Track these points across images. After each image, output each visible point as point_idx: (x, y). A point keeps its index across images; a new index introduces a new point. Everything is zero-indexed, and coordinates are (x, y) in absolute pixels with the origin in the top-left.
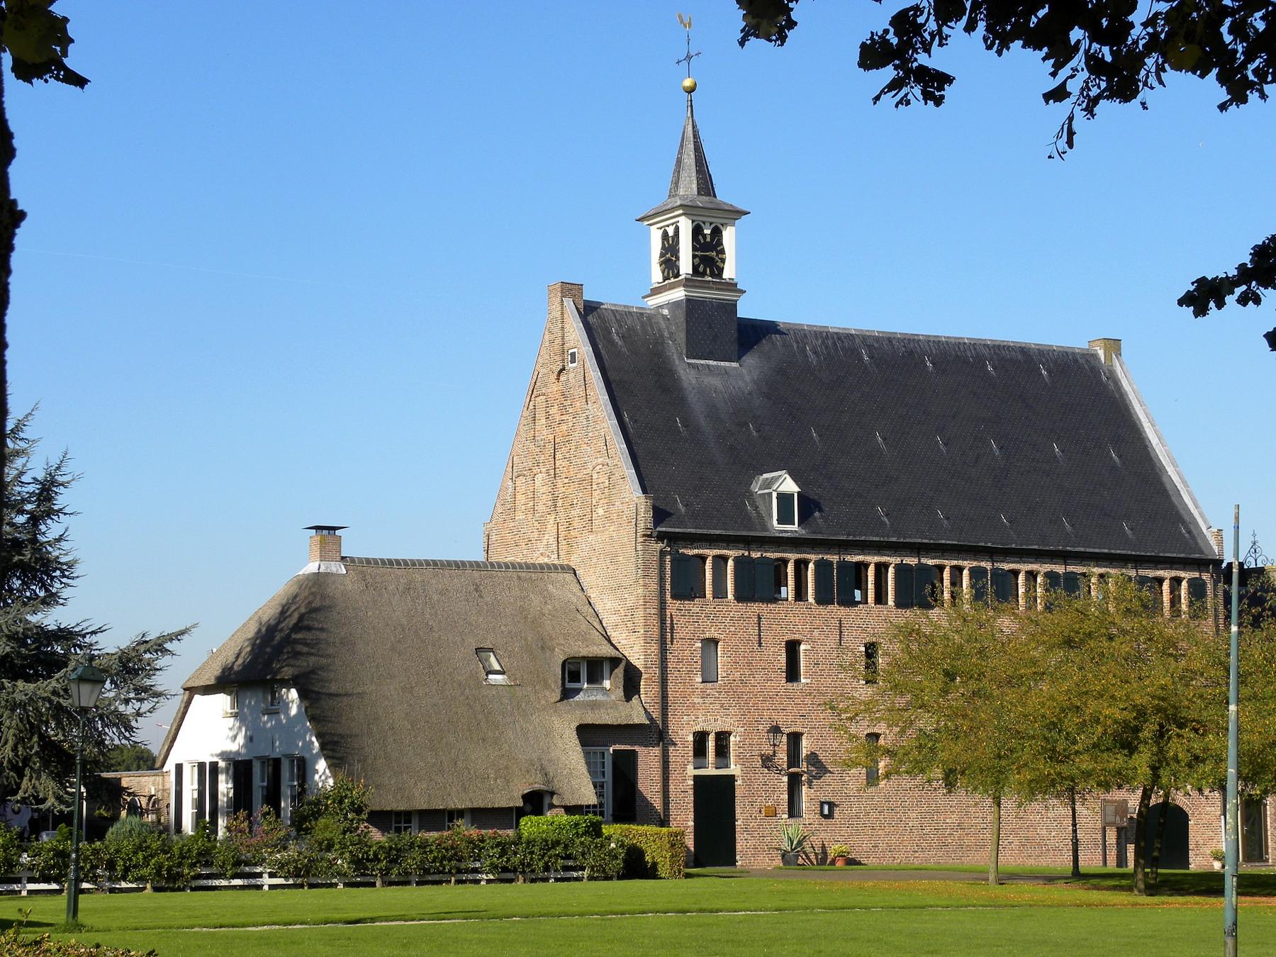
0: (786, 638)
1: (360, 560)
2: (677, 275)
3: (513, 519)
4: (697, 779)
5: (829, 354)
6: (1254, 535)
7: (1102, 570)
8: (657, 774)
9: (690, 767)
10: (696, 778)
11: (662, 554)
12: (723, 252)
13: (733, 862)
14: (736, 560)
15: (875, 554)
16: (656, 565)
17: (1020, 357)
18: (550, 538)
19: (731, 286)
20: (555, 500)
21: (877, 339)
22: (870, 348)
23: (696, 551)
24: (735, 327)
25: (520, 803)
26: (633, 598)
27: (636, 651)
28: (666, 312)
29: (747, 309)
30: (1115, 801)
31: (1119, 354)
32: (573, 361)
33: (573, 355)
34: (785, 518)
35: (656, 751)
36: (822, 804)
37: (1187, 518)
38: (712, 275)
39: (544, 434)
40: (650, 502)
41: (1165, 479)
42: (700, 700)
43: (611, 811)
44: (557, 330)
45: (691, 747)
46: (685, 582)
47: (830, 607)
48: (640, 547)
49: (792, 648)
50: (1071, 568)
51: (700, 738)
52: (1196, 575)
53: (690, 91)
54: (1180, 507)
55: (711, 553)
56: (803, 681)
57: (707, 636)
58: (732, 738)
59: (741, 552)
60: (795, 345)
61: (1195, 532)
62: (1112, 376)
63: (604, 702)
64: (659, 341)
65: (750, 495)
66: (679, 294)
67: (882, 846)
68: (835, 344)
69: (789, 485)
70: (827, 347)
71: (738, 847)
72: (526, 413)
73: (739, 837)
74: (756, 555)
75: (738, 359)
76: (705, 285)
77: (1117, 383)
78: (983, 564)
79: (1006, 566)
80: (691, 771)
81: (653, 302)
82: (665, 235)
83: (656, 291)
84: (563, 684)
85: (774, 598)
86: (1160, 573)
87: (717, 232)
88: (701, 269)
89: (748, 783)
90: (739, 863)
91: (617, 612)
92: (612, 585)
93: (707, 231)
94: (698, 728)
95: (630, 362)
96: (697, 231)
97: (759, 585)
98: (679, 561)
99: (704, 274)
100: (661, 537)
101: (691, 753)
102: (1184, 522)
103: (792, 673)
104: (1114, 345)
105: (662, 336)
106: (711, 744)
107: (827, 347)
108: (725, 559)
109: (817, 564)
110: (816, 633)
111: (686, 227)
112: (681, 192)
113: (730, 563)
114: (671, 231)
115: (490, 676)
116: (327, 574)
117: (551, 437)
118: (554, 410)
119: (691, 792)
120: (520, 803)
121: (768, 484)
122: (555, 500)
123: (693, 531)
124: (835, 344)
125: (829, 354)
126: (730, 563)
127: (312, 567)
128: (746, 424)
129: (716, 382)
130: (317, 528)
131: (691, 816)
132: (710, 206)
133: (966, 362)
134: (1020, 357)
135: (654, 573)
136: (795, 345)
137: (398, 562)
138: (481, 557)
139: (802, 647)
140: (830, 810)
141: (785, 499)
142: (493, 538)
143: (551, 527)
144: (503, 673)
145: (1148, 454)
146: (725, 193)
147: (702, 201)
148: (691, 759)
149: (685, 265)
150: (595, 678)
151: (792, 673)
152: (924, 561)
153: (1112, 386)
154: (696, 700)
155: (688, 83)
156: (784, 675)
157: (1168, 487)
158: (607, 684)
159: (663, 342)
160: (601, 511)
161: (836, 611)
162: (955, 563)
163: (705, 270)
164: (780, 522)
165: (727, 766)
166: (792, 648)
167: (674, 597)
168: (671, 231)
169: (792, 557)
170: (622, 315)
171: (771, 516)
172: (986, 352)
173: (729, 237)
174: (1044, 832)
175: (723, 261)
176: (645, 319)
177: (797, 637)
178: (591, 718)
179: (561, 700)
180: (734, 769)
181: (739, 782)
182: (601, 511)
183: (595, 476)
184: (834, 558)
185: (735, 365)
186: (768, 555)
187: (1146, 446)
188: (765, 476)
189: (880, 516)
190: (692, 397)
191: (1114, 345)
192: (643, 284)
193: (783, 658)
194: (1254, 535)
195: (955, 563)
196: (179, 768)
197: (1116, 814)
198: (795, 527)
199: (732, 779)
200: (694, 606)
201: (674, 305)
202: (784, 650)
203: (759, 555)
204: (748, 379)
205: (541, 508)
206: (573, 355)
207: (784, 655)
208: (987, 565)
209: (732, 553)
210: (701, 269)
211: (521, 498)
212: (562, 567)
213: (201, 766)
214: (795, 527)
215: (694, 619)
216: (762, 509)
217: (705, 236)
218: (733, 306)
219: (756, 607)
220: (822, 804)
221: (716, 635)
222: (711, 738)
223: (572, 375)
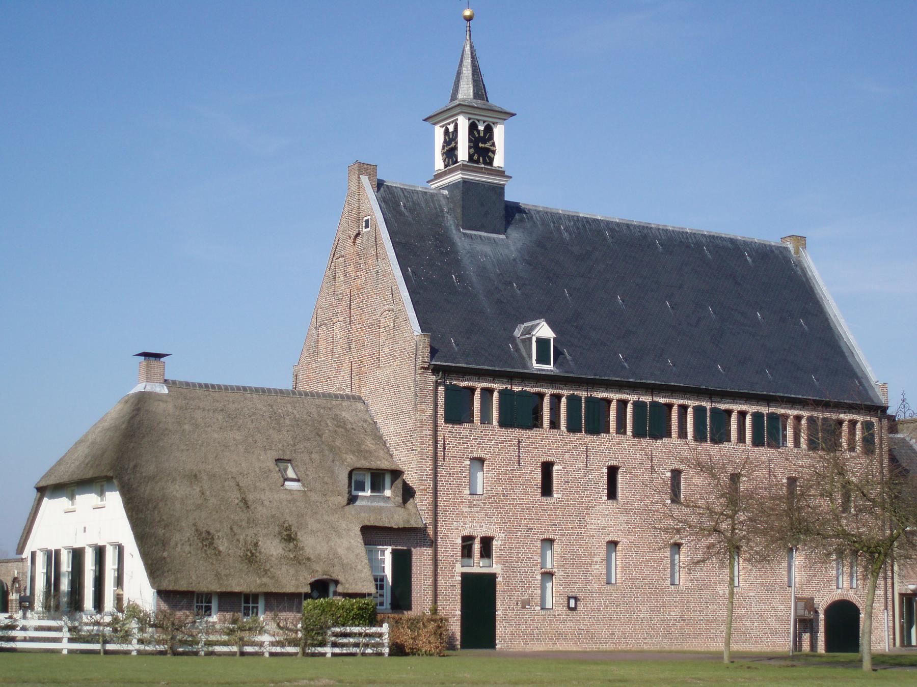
0: (542, 460)
1: (181, 383)
2: (456, 162)
3: (316, 362)
4: (464, 576)
5: (579, 234)
6: (904, 394)
7: (797, 412)
8: (429, 570)
9: (458, 565)
10: (464, 576)
11: (437, 384)
12: (493, 145)
13: (491, 644)
14: (501, 392)
15: (616, 393)
16: (431, 393)
17: (730, 245)
18: (345, 373)
19: (500, 173)
20: (349, 344)
21: (618, 224)
22: (612, 230)
23: (466, 384)
24: (503, 206)
25: (307, 589)
26: (412, 421)
27: (415, 473)
28: (446, 192)
29: (510, 196)
30: (804, 599)
31: (804, 247)
32: (367, 227)
33: (367, 221)
34: (543, 358)
35: (428, 551)
36: (569, 598)
37: (860, 375)
38: (485, 163)
39: (342, 288)
40: (427, 340)
41: (842, 345)
42: (468, 509)
43: (389, 601)
44: (353, 201)
45: (459, 548)
46: (458, 410)
47: (578, 435)
48: (418, 378)
49: (547, 468)
50: (773, 410)
51: (468, 541)
52: (868, 418)
53: (469, 19)
54: (854, 366)
55: (480, 385)
56: (555, 496)
57: (475, 455)
58: (494, 542)
59: (505, 386)
60: (552, 225)
61: (866, 385)
62: (799, 264)
63: (382, 506)
64: (437, 218)
65: (513, 339)
66: (457, 177)
67: (618, 634)
68: (584, 226)
69: (544, 331)
70: (578, 228)
71: (498, 632)
72: (329, 273)
73: (499, 625)
74: (517, 389)
75: (505, 232)
76: (479, 171)
77: (803, 270)
78: (704, 404)
79: (723, 406)
80: (459, 569)
81: (434, 185)
82: (447, 132)
83: (439, 176)
84: (350, 492)
85: (536, 423)
86: (842, 416)
87: (489, 129)
88: (476, 157)
89: (507, 580)
90: (498, 646)
91: (398, 434)
92: (395, 403)
93: (481, 128)
94: (466, 533)
95: (416, 231)
96: (473, 127)
97: (521, 414)
98: (451, 392)
99: (477, 162)
100: (436, 370)
101: (459, 554)
102: (858, 378)
103: (547, 489)
104: (801, 241)
105: (442, 211)
106: (477, 547)
107: (578, 228)
108: (490, 391)
109: (569, 398)
110: (567, 456)
111: (463, 123)
112: (460, 96)
113: (496, 395)
114: (451, 128)
115: (287, 483)
116: (150, 393)
117: (348, 291)
118: (351, 269)
119: (459, 587)
120: (307, 589)
121: (529, 331)
122: (349, 344)
123: (464, 365)
124: (584, 226)
125: (579, 234)
126: (496, 395)
127: (140, 388)
128: (511, 283)
129: (487, 249)
130: (146, 355)
131: (459, 606)
132: (484, 107)
133: (688, 247)
134: (730, 245)
135: (430, 399)
136: (552, 225)
137: (213, 386)
138: (288, 386)
139: (555, 468)
140: (576, 604)
141: (543, 343)
142: (300, 377)
143: (346, 366)
144: (298, 480)
145: (829, 324)
146: (495, 99)
147: (479, 103)
148: (459, 558)
149: (463, 154)
150: (377, 486)
151: (547, 489)
152: (656, 399)
153: (800, 272)
154: (464, 509)
155: (467, 13)
156: (539, 490)
157: (845, 350)
158: (388, 493)
159: (443, 216)
160: (386, 350)
161: (583, 438)
162: (681, 402)
163: (479, 158)
164: (538, 361)
165: (491, 566)
166: (547, 468)
167: (448, 420)
168: (451, 128)
169: (548, 391)
170: (408, 194)
171: (530, 357)
172: (704, 240)
173: (499, 133)
174: (748, 623)
175: (494, 152)
176: (430, 197)
177: (550, 459)
178: (372, 521)
179: (348, 504)
180: (496, 568)
181: (499, 579)
182: (386, 350)
183: (383, 320)
184: (583, 394)
185: (502, 237)
186: (527, 389)
187: (827, 319)
188: (526, 324)
189: (621, 362)
190: (466, 261)
191: (801, 241)
192: (429, 166)
193: (539, 476)
194: (904, 394)
195: (681, 402)
196: (33, 554)
197: (805, 608)
198: (551, 367)
199: (493, 577)
200: (464, 429)
201: (451, 187)
202: (539, 470)
203: (520, 389)
204: (513, 248)
205: (338, 350)
206: (367, 221)
207: (540, 474)
208: (707, 405)
209: (497, 386)
210: (476, 157)
211: (322, 345)
212: (354, 397)
213: (48, 554)
214: (551, 367)
215: (462, 440)
216: (523, 351)
217: (479, 132)
218: (500, 190)
219: (516, 433)
220: (569, 598)
221: (482, 455)
222: (477, 541)
223: (365, 238)
